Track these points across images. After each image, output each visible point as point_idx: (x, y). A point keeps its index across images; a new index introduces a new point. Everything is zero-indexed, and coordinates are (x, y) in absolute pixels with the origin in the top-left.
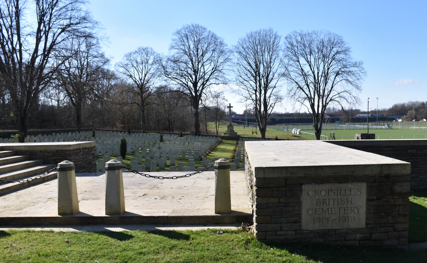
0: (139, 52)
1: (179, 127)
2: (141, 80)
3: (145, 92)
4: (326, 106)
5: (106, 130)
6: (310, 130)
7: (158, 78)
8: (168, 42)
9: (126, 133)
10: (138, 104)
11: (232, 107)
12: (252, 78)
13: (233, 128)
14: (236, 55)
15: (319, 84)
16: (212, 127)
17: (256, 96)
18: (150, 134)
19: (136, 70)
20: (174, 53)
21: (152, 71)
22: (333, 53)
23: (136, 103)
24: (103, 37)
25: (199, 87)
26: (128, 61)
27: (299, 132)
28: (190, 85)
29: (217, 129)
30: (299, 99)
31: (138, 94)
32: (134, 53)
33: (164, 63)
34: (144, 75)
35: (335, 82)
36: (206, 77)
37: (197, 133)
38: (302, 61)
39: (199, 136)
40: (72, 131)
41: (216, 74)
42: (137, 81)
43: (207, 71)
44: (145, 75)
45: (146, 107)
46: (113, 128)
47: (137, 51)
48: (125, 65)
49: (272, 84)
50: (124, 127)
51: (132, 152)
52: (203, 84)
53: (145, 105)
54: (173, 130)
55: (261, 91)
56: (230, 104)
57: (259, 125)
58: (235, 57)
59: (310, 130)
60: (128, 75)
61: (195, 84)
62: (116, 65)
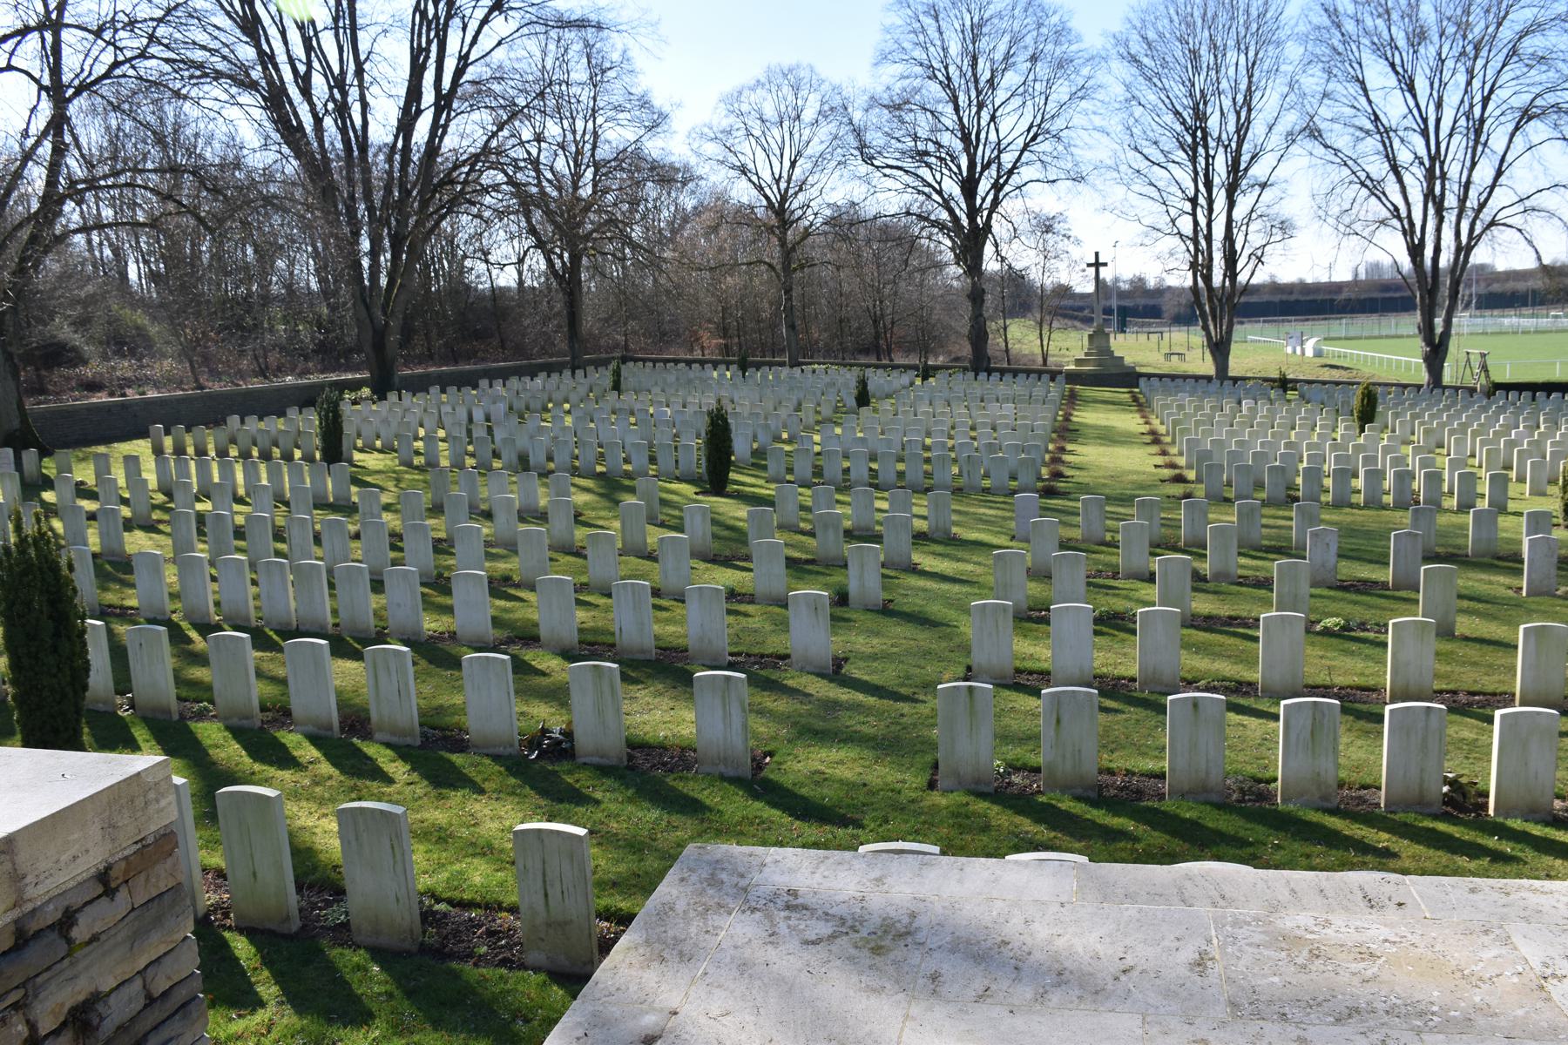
0: (767, 86)
1: (909, 338)
2: (778, 181)
3: (793, 222)
4: (1469, 249)
5: (666, 361)
6: (1340, 339)
7: (837, 174)
8: (871, 39)
9: (734, 367)
10: (770, 265)
11: (1105, 264)
12: (1180, 155)
13: (1108, 341)
14: (1124, 70)
15: (1442, 163)
16: (1022, 337)
17: (1196, 223)
18: (814, 371)
19: (759, 151)
20: (891, 78)
21: (814, 149)
22: (1506, 33)
23: (765, 263)
24: (636, 23)
25: (983, 200)
26: (732, 119)
27: (1314, 349)
28: (952, 187)
29: (1045, 343)
30: (1358, 227)
31: (771, 230)
32: (753, 89)
33: (857, 116)
34: (787, 164)
35: (1509, 158)
36: (1008, 159)
37: (981, 363)
38: (1378, 75)
39: (989, 372)
40: (550, 369)
41: (1043, 146)
42: (764, 185)
43: (1010, 139)
44: (793, 164)
45: (799, 274)
46: (691, 351)
47: (763, 80)
48: (722, 132)
49: (1259, 171)
50: (726, 345)
51: (755, 453)
52: (997, 187)
53: (795, 269)
54: (889, 352)
55: (1210, 202)
56: (1097, 254)
57: (1205, 328)
58: (1115, 78)
59: (1340, 339)
60: (733, 167)
61: (969, 187)
62: (694, 135)
